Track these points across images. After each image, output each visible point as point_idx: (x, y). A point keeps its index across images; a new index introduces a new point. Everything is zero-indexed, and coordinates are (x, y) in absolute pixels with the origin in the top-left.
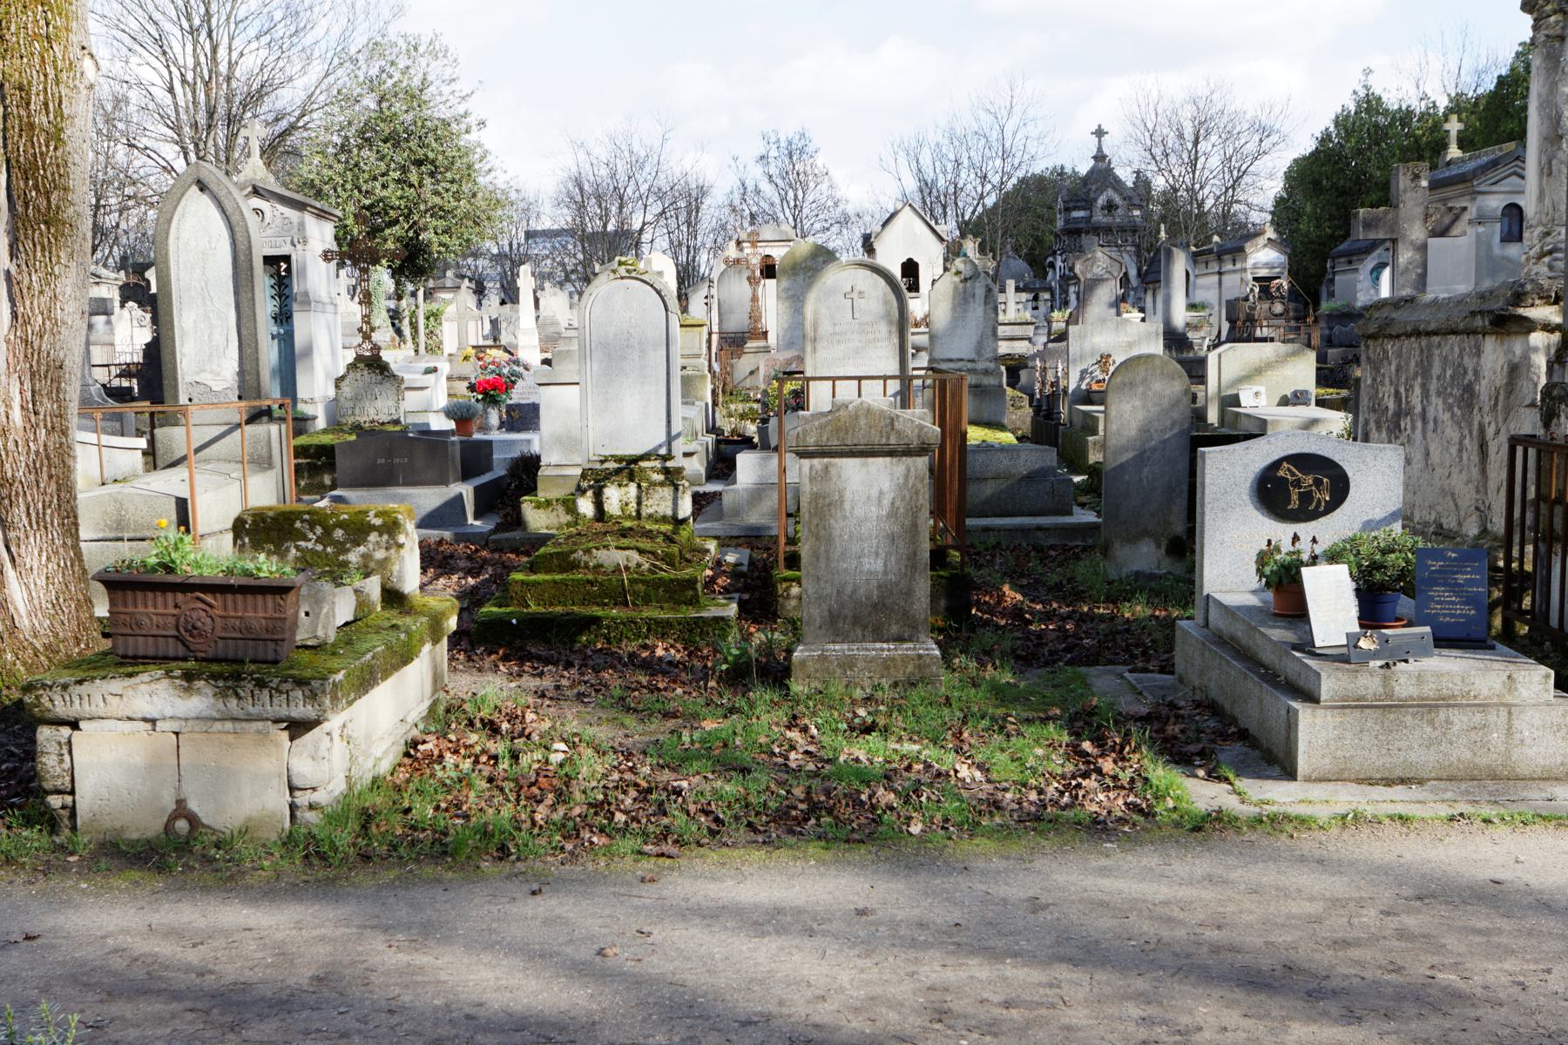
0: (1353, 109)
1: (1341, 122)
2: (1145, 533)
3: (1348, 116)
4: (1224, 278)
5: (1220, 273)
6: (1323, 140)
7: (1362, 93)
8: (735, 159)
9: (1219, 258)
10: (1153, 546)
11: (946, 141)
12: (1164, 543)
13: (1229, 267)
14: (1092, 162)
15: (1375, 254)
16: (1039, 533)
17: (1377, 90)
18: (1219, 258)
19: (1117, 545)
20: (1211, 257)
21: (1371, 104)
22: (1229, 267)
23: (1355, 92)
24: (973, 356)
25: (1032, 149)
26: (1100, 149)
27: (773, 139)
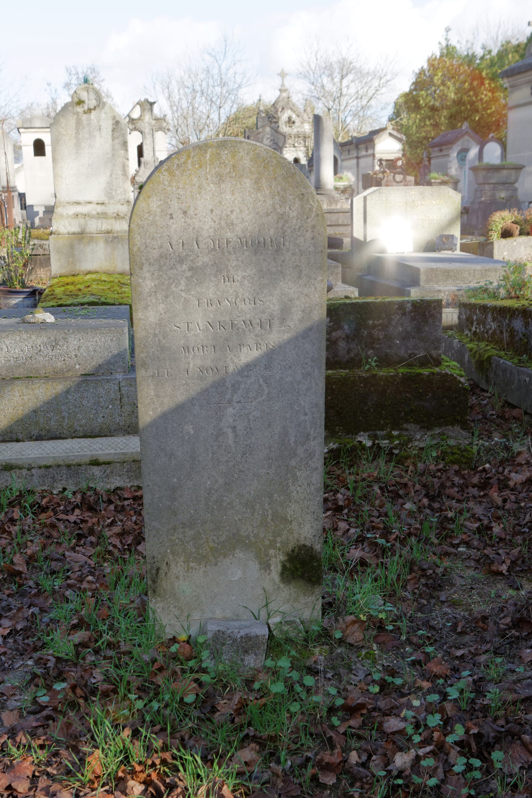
0: (438, 55)
1: (431, 62)
2: (236, 542)
3: (436, 58)
4: (361, 161)
5: (358, 158)
6: (420, 74)
7: (444, 44)
8: (49, 84)
9: (357, 148)
10: (254, 566)
11: (187, 77)
12: (277, 560)
13: (363, 153)
14: (278, 93)
15: (460, 142)
16: (96, 471)
17: (453, 42)
18: (357, 148)
19: (177, 568)
20: (352, 147)
21: (449, 52)
22: (363, 153)
23: (440, 43)
24: (103, 199)
25: (238, 80)
26: (283, 85)
27: (74, 72)
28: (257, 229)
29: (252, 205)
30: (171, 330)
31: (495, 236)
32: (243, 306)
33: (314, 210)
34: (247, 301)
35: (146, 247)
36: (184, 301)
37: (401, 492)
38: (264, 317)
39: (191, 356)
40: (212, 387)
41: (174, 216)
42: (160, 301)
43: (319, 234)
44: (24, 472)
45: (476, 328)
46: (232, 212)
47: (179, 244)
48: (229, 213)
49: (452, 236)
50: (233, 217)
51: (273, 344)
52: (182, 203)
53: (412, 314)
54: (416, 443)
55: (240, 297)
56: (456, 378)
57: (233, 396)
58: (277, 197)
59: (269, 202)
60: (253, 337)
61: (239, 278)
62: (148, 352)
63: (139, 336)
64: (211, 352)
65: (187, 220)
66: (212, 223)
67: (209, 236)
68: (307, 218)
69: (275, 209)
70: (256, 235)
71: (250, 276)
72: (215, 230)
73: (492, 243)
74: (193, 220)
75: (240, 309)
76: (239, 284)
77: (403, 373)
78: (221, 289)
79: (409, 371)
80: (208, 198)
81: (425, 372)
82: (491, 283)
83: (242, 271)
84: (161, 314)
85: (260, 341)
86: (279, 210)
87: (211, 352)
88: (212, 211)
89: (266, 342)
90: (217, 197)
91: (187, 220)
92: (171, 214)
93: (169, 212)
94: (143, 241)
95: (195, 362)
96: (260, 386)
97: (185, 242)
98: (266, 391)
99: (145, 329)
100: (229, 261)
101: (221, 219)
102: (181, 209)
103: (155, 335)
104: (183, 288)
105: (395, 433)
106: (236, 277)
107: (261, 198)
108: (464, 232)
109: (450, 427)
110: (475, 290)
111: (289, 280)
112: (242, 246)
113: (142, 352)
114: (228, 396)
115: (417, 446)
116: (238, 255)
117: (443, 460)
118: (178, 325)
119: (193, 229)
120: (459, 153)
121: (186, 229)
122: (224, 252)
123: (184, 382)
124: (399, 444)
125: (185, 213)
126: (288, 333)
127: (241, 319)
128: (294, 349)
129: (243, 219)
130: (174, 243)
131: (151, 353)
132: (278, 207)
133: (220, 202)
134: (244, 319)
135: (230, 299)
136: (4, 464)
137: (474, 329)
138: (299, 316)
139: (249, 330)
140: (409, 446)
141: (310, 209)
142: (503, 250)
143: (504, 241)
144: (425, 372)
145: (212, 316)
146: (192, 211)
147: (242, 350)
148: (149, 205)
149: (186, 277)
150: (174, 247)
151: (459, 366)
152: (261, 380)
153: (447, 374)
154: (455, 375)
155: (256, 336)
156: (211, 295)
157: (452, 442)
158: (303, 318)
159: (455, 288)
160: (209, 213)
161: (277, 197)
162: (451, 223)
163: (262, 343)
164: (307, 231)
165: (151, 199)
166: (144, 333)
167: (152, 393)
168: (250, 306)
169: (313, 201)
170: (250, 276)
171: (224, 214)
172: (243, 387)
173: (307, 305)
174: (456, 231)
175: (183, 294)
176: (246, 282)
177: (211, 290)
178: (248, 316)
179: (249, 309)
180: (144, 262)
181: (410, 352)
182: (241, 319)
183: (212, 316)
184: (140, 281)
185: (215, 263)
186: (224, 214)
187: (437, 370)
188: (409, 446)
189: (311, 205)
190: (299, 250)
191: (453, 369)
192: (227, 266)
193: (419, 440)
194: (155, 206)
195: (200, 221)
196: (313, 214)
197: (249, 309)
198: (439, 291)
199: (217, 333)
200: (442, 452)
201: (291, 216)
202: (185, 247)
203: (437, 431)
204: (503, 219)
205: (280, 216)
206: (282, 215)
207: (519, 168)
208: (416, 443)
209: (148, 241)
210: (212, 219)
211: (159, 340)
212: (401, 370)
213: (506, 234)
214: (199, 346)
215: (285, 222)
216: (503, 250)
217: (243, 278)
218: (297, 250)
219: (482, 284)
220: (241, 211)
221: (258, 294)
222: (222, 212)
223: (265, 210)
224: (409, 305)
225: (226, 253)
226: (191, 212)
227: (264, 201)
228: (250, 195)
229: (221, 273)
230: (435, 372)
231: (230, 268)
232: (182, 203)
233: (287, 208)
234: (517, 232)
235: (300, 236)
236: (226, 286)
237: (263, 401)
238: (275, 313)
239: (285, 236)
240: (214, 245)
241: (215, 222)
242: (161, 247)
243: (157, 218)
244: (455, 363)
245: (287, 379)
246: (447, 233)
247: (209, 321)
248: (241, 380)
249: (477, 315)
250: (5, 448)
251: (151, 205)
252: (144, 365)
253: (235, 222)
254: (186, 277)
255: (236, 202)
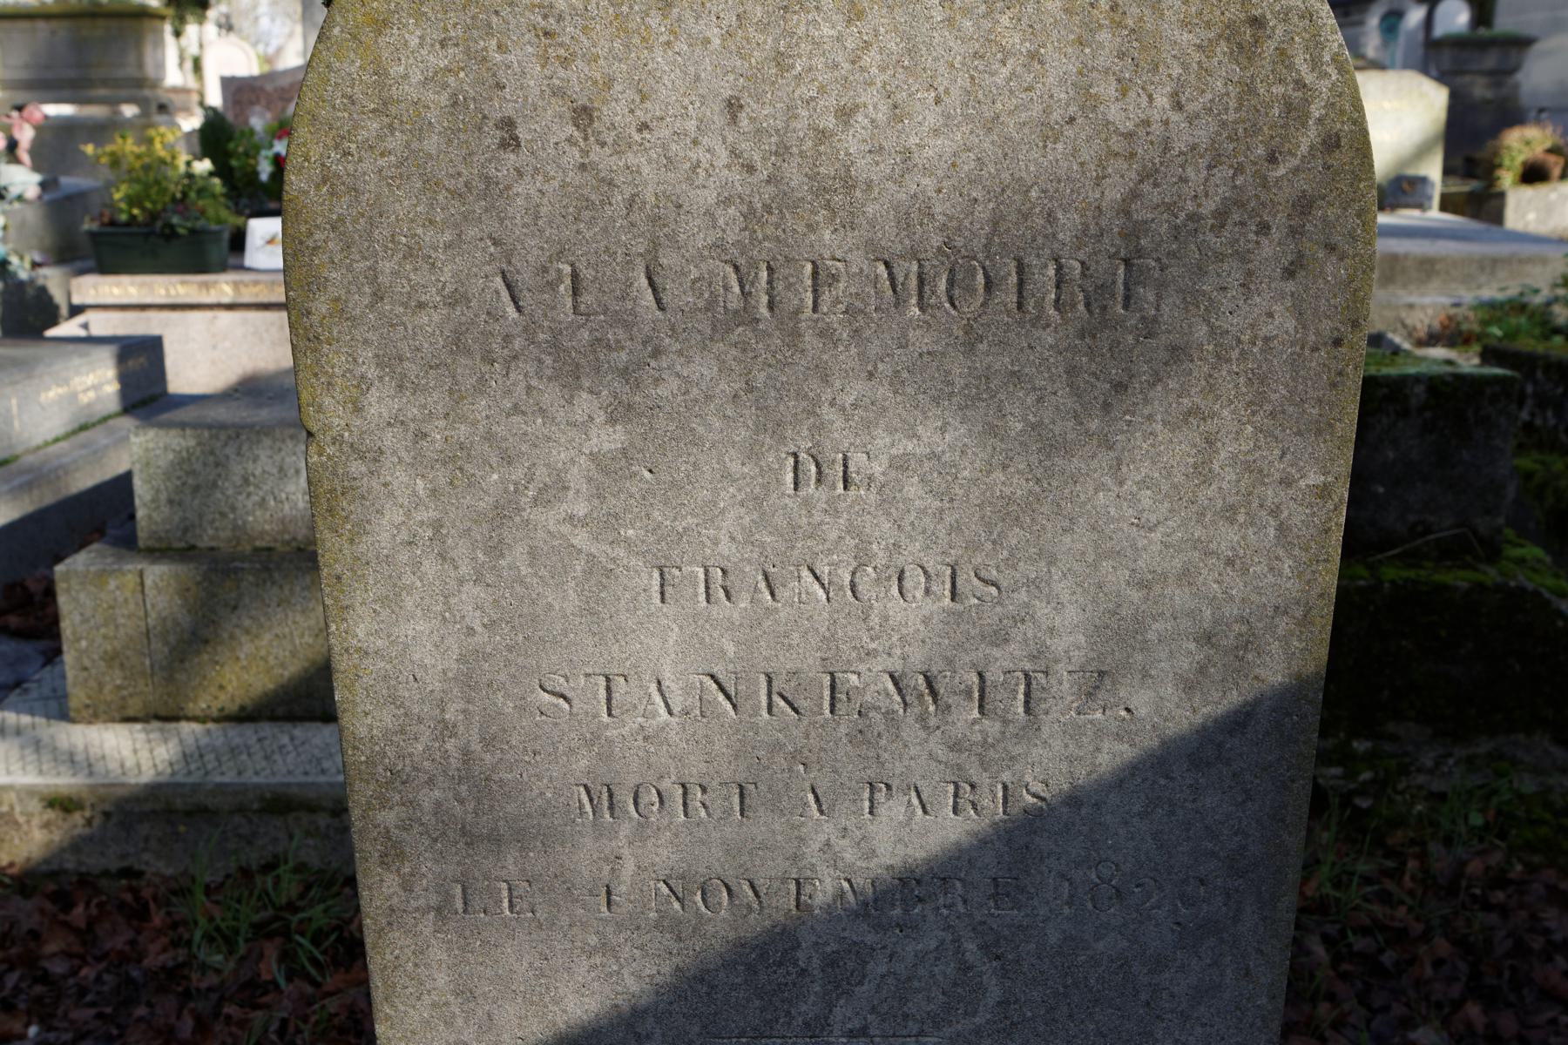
28: (983, 213)
29: (963, 80)
30: (522, 709)
31: (1507, 179)
32: (895, 606)
33: (1316, 111)
34: (915, 579)
35: (378, 296)
36: (588, 573)
37: (1388, 958)
38: (1003, 660)
39: (625, 829)
40: (729, 965)
41: (522, 134)
42: (465, 570)
43: (1331, 248)
44: (323, 820)
45: (1533, 415)
46: (846, 114)
47: (552, 286)
48: (829, 122)
49: (1423, 180)
50: (852, 142)
51: (1038, 788)
52: (565, 62)
53: (1428, 414)
54: (1421, 779)
55: (881, 560)
56: (1548, 602)
57: (831, 1007)
58: (1104, 36)
59: (1061, 65)
60: (941, 752)
61: (877, 469)
62: (411, 803)
63: (362, 731)
64: (728, 812)
65: (597, 153)
66: (736, 176)
67: (719, 246)
68: (1272, 159)
69: (1089, 102)
70: (977, 245)
71: (933, 456)
72: (750, 214)
73: (1502, 196)
74: (631, 159)
75: (875, 620)
76: (873, 497)
77: (1393, 582)
78: (779, 520)
79: (1411, 574)
80: (714, 35)
81: (1458, 579)
82: (1537, 291)
83: (891, 431)
84: (471, 631)
85: (974, 772)
86: (1114, 112)
87: (728, 812)
88: (733, 107)
89: (1006, 776)
90: (763, 27)
91: (597, 153)
92: (508, 124)
93: (499, 108)
94: (361, 266)
95: (642, 857)
96: (965, 968)
97: (587, 274)
98: (995, 992)
99: (394, 700)
100: (826, 380)
101: (782, 151)
102: (557, 92)
103: (446, 729)
104: (581, 509)
105: (1361, 746)
106: (858, 459)
107: (1014, 40)
108: (1447, 171)
109: (1521, 737)
110: (1492, 305)
111: (1143, 484)
112: (899, 302)
113: (384, 804)
114: (808, 1008)
115: (1420, 787)
116: (874, 349)
117: (1502, 836)
118: (560, 683)
119: (631, 202)
120: (1384, 18)
121: (590, 205)
122: (796, 334)
123: (593, 940)
124: (1373, 781)
125: (583, 115)
126: (1118, 737)
127: (879, 664)
128: (1142, 815)
129: (907, 154)
130: (525, 278)
131: (427, 805)
132: (1108, 89)
133: (781, 60)
134: (896, 665)
135: (824, 570)
136: (268, 795)
137: (1524, 415)
138: (1185, 664)
139: (922, 719)
140: (1401, 786)
141: (1289, 107)
142: (1527, 210)
143: (1528, 192)
144: (1458, 579)
145: (731, 649)
146: (621, 108)
147: (881, 810)
148: (380, 72)
149: (593, 456)
150: (527, 300)
151: (1548, 559)
152: (971, 946)
153: (1523, 590)
154: (1547, 595)
155: (955, 746)
156: (725, 547)
157: (1528, 785)
158: (1202, 670)
159: (1446, 301)
160: (719, 120)
161: (1104, 36)
162: (1421, 152)
163: (983, 779)
164: (1264, 228)
165: (391, 36)
166: (387, 718)
167: (442, 979)
168: (929, 606)
169: (1315, 64)
170: (933, 456)
171: (800, 125)
172: (882, 969)
173: (1232, 611)
174: (1433, 170)
175: (581, 539)
176: (913, 488)
177: (728, 523)
178: (917, 656)
179: (926, 621)
180: (372, 373)
181: (1412, 518)
182: (879, 664)
183: (731, 649)
184: (357, 467)
185: (750, 389)
186: (800, 125)
187: (1491, 575)
188: (1401, 786)
189: (1300, 84)
190: (1212, 330)
191: (1535, 570)
192: (816, 402)
193: (1431, 772)
194: (416, 77)
195: (670, 163)
196: (1308, 138)
197: (926, 621)
198: (1411, 306)
199: (755, 728)
200: (1499, 813)
201: (1179, 146)
202: (587, 299)
203: (1484, 746)
204: (1528, 143)
205: (1116, 144)
206: (1129, 135)
207: (1521, 43)
208: (1421, 779)
209: (387, 266)
210: (734, 153)
211: (466, 752)
212: (1390, 573)
213: (1533, 174)
214: (665, 784)
215: (1144, 176)
216: (1527, 210)
217: (900, 464)
218: (1202, 331)
219: (1513, 292)
220: (898, 114)
221: (973, 547)
222: (791, 113)
223: (1036, 110)
224: (1420, 389)
225: (809, 337)
226: (617, 112)
227: (1033, 55)
228: (950, 21)
229: (783, 439)
230: (1489, 583)
231: (827, 413)
232: (565, 62)
233: (1162, 101)
234: (1557, 171)
235: (1220, 257)
236: (807, 503)
237: (977, 1031)
238: (1058, 645)
239: (1140, 252)
240: (745, 294)
241: (751, 169)
242: (456, 299)
243: (432, 143)
244: (1538, 552)
245: (1100, 946)
246: (1411, 172)
247: (717, 670)
248: (870, 939)
249: (1535, 383)
250: (285, 740)
251: (396, 70)
252: (393, 853)
253: (863, 167)
254: (593, 456)
255: (871, 59)
